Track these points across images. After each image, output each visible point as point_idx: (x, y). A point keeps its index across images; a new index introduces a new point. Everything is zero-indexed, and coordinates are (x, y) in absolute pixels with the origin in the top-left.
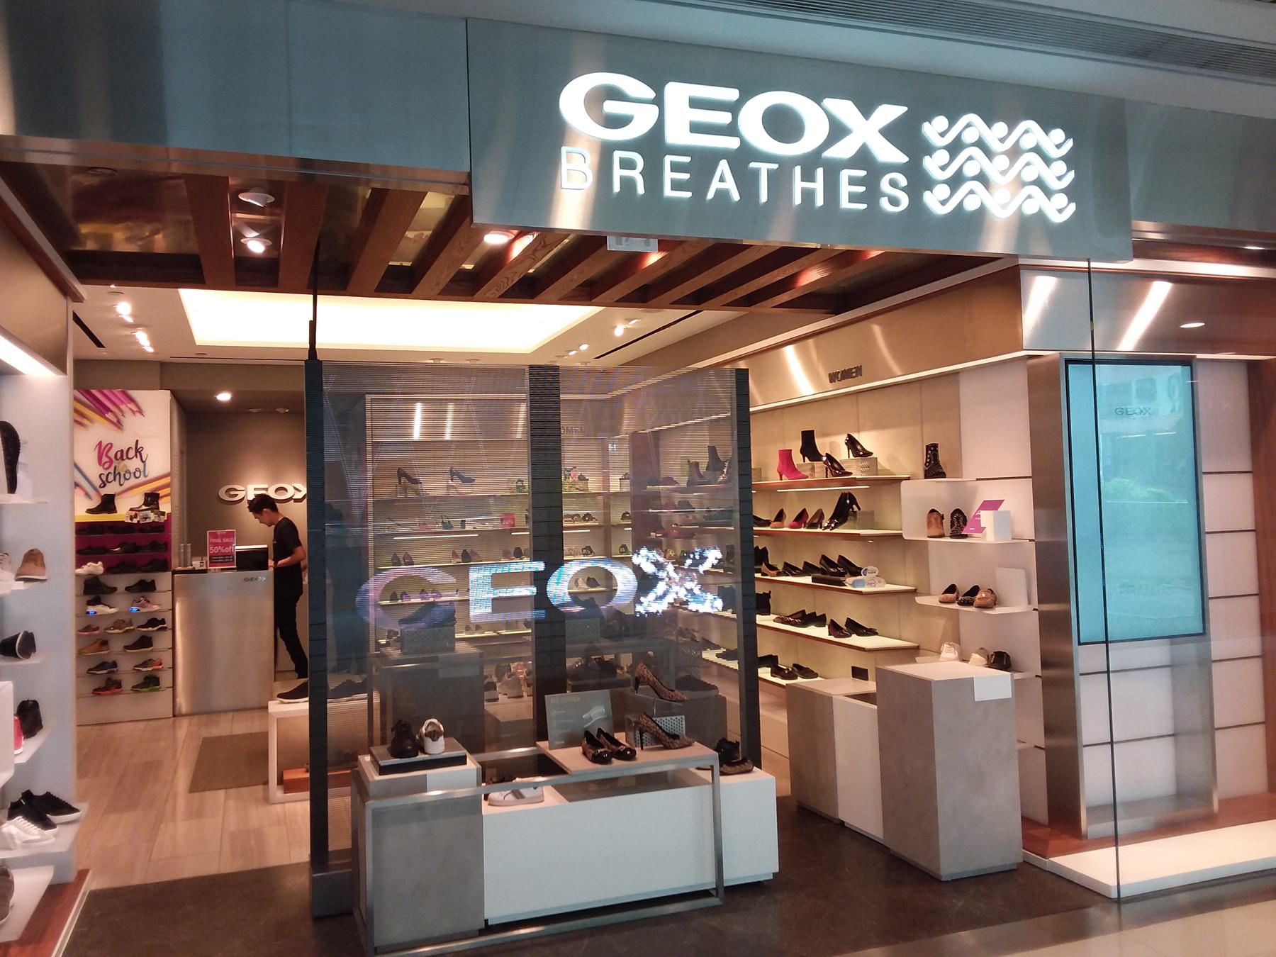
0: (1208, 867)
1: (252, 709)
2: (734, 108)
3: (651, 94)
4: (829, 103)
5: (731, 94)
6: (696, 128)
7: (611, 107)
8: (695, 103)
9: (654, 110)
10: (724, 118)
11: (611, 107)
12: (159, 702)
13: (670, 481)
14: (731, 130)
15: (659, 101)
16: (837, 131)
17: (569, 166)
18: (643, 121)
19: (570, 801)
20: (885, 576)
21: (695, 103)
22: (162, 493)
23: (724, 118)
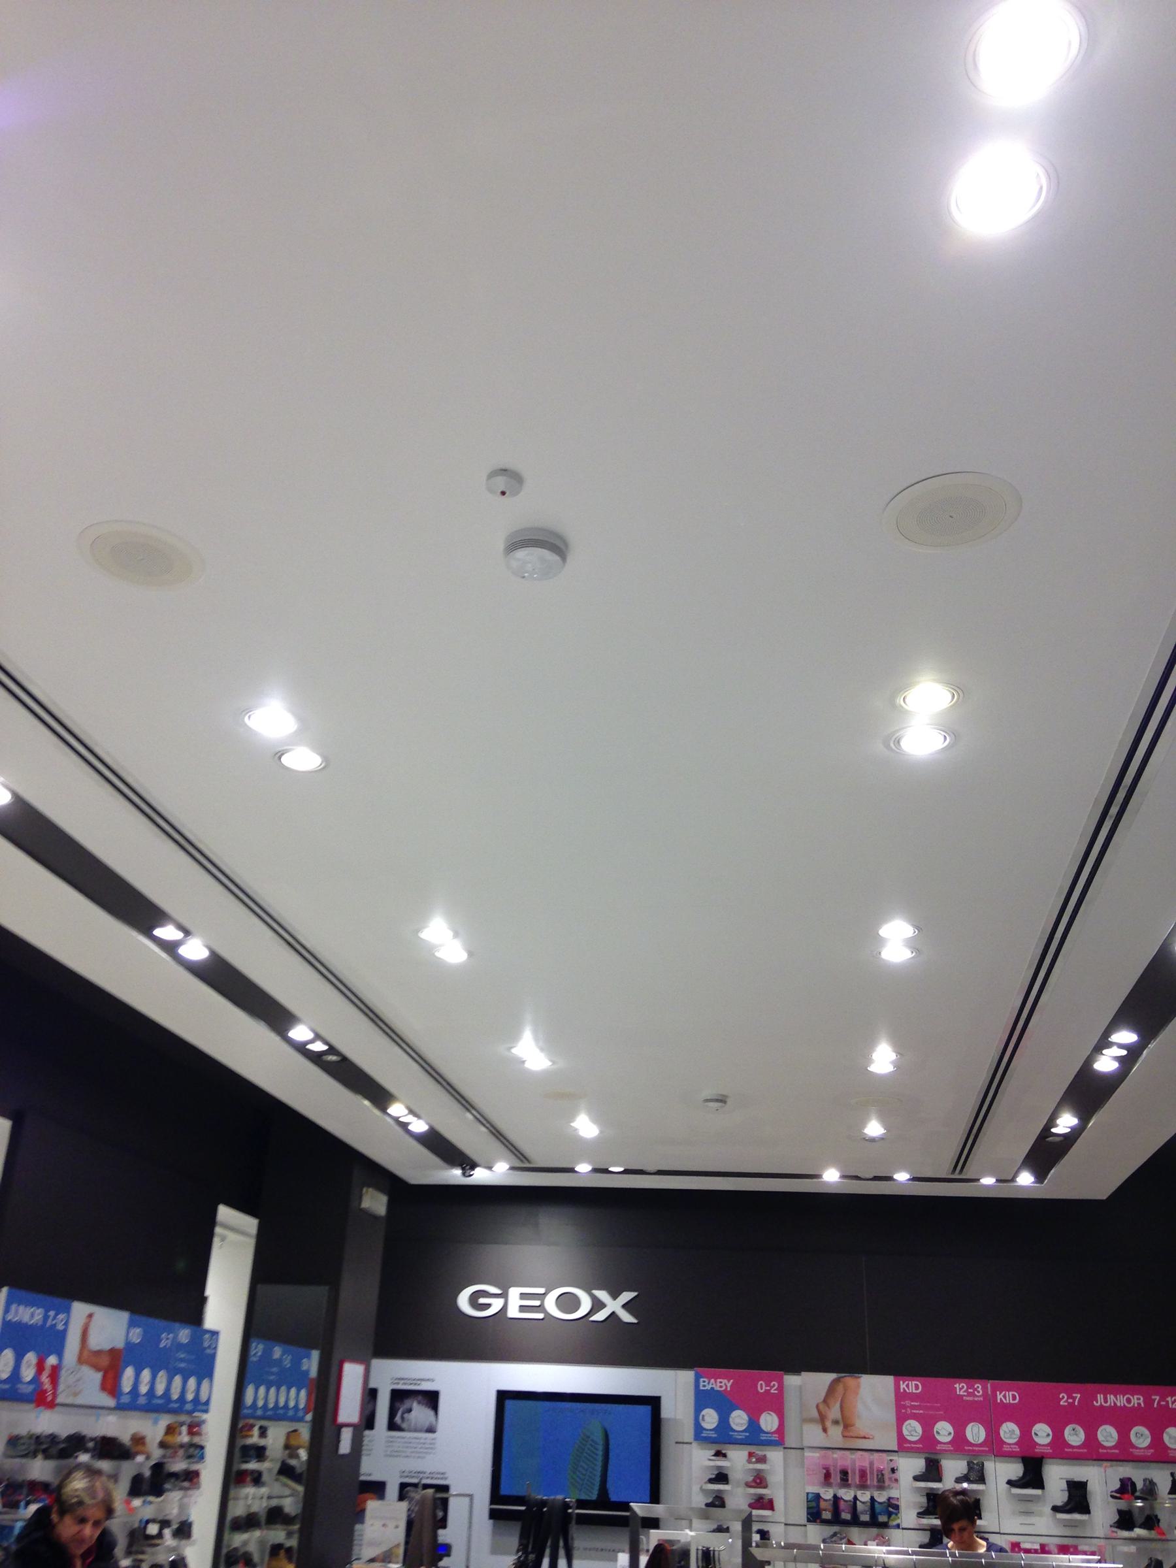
7: (482, 1301)
8: (523, 1296)
11: (482, 1301)
14: (540, 1308)
15: (504, 1295)
16: (598, 1305)
18: (496, 1305)
21: (523, 1296)
23: (537, 1303)
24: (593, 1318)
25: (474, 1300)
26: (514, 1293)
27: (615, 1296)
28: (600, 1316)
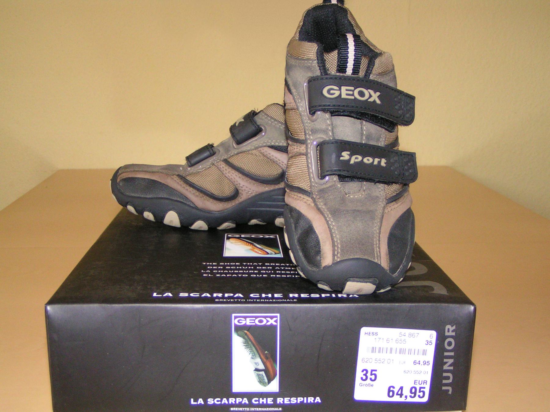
0: (470, 378)
1: (324, 66)
2: (353, 91)
3: (337, 88)
4: (369, 90)
5: (352, 88)
6: (347, 95)
7: (332, 92)
8: (347, 90)
9: (339, 92)
10: (351, 93)
11: (332, 92)
13: (308, 59)
14: (353, 95)
15: (340, 89)
16: (370, 96)
18: (337, 93)
19: (308, 13)
21: (347, 90)
22: (332, 58)
23: (351, 93)
24: (369, 100)
25: (329, 92)
27: (374, 101)
28: (269, 324)
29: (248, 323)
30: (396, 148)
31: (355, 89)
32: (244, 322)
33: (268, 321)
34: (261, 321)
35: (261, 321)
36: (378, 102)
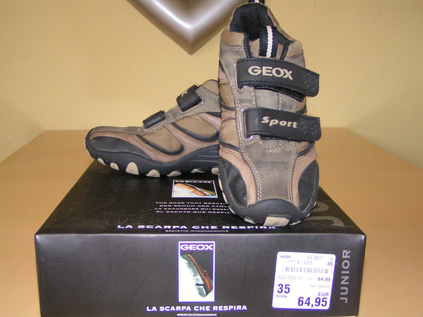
0: (365, 259)
2: (272, 70)
3: (260, 68)
4: (284, 69)
5: (271, 68)
6: (267, 73)
7: (255, 71)
8: (267, 69)
10: (270, 71)
11: (255, 71)
12: (247, 105)
14: (271, 73)
15: (262, 69)
16: (285, 74)
17: (313, 257)
18: (259, 72)
20: (272, 196)
21: (267, 69)
23: (270, 71)
24: (284, 77)
25: (253, 70)
26: (264, 68)
27: (288, 78)
28: (207, 249)
29: (191, 249)
30: (304, 114)
31: (273, 68)
32: (187, 248)
33: (206, 247)
34: (200, 247)
35: (200, 247)
36: (291, 78)
